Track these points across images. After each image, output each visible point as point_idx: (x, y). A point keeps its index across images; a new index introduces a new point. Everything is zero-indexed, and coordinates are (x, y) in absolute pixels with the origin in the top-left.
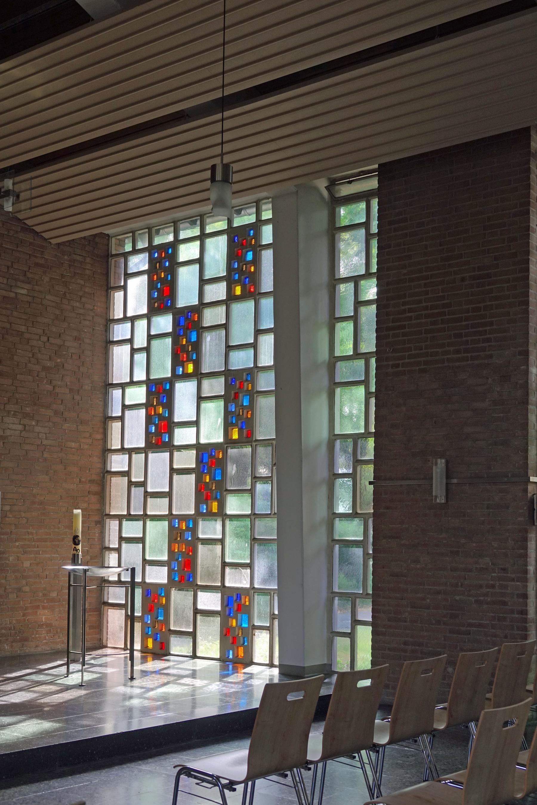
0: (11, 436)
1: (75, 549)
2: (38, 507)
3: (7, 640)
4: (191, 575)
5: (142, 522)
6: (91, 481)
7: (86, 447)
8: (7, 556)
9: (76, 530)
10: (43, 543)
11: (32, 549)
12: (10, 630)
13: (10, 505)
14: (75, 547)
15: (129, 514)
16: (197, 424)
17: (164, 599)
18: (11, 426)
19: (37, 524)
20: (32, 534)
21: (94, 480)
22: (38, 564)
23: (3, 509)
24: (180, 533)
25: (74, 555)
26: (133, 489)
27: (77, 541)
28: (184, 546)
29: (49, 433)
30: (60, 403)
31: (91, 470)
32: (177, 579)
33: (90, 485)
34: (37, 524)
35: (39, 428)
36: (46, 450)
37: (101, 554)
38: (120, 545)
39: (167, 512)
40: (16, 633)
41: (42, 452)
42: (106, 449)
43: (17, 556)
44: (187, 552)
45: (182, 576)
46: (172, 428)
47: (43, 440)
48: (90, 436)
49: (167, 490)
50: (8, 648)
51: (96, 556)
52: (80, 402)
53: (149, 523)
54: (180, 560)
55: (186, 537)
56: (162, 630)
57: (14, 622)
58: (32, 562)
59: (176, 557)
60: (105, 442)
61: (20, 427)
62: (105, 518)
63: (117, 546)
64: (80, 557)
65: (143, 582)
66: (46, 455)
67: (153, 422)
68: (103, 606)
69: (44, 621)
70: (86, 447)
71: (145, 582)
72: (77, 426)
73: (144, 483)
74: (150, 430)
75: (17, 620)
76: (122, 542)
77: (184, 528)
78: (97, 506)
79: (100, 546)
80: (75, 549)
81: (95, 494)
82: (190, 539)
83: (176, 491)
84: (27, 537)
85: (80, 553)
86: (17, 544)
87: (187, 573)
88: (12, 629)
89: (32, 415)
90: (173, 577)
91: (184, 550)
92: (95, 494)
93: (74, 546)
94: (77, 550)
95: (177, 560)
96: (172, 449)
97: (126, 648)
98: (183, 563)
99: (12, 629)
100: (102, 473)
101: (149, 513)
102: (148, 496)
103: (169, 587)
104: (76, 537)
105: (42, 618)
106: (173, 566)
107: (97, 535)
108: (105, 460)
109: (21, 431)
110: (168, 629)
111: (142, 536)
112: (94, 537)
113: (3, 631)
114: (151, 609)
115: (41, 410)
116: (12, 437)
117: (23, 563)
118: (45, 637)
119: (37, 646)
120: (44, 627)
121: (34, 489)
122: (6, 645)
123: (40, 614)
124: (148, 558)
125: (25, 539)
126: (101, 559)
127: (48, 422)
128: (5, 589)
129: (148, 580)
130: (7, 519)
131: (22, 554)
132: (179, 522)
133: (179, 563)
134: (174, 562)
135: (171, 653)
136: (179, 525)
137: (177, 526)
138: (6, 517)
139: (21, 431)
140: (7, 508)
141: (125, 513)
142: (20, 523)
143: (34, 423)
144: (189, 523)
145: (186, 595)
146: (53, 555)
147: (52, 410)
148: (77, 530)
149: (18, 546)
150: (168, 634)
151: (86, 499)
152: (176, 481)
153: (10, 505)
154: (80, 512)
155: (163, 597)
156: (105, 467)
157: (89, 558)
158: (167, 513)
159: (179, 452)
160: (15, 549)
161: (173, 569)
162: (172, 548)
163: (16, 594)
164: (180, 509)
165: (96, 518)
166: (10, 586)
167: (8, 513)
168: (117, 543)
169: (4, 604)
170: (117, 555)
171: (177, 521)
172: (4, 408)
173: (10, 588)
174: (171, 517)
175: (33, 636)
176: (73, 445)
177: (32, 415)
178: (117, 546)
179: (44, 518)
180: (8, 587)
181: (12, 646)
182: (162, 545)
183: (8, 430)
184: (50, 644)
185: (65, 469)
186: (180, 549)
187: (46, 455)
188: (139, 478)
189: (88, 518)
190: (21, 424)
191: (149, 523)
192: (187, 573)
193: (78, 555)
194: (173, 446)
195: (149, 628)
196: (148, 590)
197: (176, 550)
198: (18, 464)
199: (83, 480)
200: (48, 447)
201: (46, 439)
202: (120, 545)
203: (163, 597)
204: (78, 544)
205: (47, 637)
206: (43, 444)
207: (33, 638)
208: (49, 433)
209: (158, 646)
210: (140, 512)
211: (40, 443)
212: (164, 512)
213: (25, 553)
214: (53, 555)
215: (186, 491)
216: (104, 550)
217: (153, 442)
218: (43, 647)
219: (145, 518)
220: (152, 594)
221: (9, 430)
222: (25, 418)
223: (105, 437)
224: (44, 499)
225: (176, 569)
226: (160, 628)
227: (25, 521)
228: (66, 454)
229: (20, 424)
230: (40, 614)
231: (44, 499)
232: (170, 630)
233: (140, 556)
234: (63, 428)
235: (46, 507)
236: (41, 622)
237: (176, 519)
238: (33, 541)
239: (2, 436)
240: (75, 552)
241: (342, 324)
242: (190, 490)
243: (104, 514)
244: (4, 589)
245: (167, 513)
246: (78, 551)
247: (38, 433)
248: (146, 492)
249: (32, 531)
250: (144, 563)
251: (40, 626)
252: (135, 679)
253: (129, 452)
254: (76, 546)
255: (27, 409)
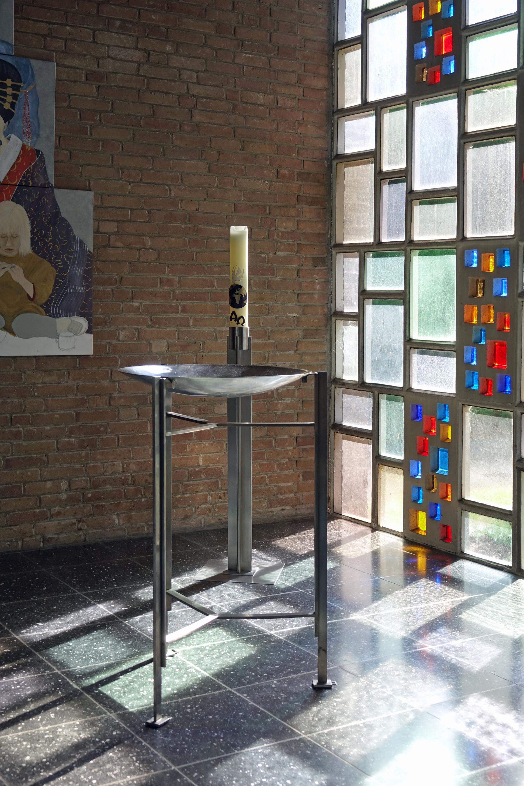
0: (116, 73)
1: (234, 316)
2: (183, 226)
3: (118, 505)
4: (509, 379)
5: (404, 258)
6: (302, 176)
7: (290, 103)
8: (112, 329)
9: (237, 273)
10: (196, 303)
11: (171, 315)
12: (123, 484)
13: (118, 222)
14: (234, 313)
15: (378, 243)
16: (518, 22)
17: (450, 428)
18: (114, 52)
19: (182, 262)
20: (170, 282)
21: (309, 174)
22: (184, 347)
23: (102, 230)
24: (484, 281)
25: (233, 329)
26: (386, 188)
27: (237, 298)
28: (492, 311)
29: (206, 71)
30: (230, 8)
31: (301, 151)
32: (476, 387)
33: (300, 183)
34: (182, 262)
35: (182, 59)
36: (200, 107)
37: (326, 325)
38: (362, 307)
39: (453, 234)
40: (137, 491)
41: (190, 110)
42: (335, 110)
43: (136, 329)
44: (498, 327)
45: (488, 381)
46: (463, 40)
47: (191, 86)
48: (300, 81)
49: (453, 183)
50: (121, 523)
51: (317, 330)
52: (275, 8)
53: (417, 260)
54: (483, 342)
55: (495, 290)
56: (447, 496)
57: (133, 467)
58: (171, 341)
59: (474, 338)
60: (333, 94)
61: (138, 55)
62: (334, 252)
63: (356, 310)
64: (247, 334)
65: (407, 388)
66: (198, 117)
67: (422, 36)
68: (332, 432)
69: (201, 464)
70: (290, 103)
71: (410, 389)
72: (269, 59)
73: (407, 174)
74: (416, 56)
75: (139, 463)
76: (366, 301)
77: (492, 270)
78: (318, 228)
79: (325, 310)
80: (234, 316)
81: (311, 203)
82: (504, 294)
83: (473, 185)
84: (158, 289)
85: (246, 325)
86: (136, 304)
87: (498, 375)
88: (130, 482)
89: (164, 29)
90: (468, 382)
91: (492, 320)
92: (313, 202)
93: (232, 309)
94: (237, 319)
95: (477, 342)
96: (464, 88)
97: (375, 526)
98: (489, 351)
99: (130, 482)
100: (327, 159)
101: (416, 237)
102: (414, 202)
103: (460, 404)
104: (236, 289)
105: (197, 458)
106: (467, 357)
107: (318, 287)
108: (332, 133)
109: (139, 64)
110: (459, 498)
111: (402, 288)
112: (311, 292)
113: (108, 486)
114: (423, 451)
115: (185, 20)
116: (119, 76)
117: (150, 344)
118: (206, 499)
119: (186, 517)
120: (203, 477)
121: (172, 188)
122: (114, 517)
123: (192, 450)
124: (415, 335)
125: (155, 295)
126: (328, 335)
127: (202, 46)
128: (111, 398)
129: (416, 385)
130: (111, 251)
131: (148, 326)
132: (479, 258)
133: (481, 350)
134: (470, 348)
135: (467, 551)
136: (479, 262)
137: (475, 265)
138: (108, 246)
139: (139, 64)
140: (112, 227)
141: (370, 240)
142: (141, 259)
143: (168, 48)
144: (504, 258)
145: (497, 426)
146: (219, 329)
147: (211, 22)
148: (238, 272)
149: (138, 308)
150: (459, 509)
151: (293, 212)
152: (474, 161)
153: (118, 222)
154: (243, 232)
155: (447, 424)
156: (332, 146)
157: (301, 334)
158: (454, 236)
159: (479, 95)
160: (132, 316)
161: (469, 364)
162: (466, 317)
163: (137, 409)
164: (482, 227)
165: (316, 253)
166: (120, 392)
167: (113, 239)
168: (356, 303)
169: (109, 430)
170: (356, 329)
171: (475, 254)
172: (98, 12)
173: (121, 397)
174: (462, 245)
175: (178, 496)
176: (261, 98)
177: (164, 29)
178: (356, 310)
179: (198, 250)
180: (116, 395)
181: (129, 518)
182: (444, 309)
183: (109, 59)
184: (216, 512)
185: (243, 149)
186: (483, 319)
187: (198, 117)
188: (397, 163)
189: (298, 252)
190: (140, 50)
191: (417, 260)
192: (498, 375)
193: (241, 329)
194: (467, 81)
195: (419, 488)
196: (417, 406)
197: (475, 321)
198: (134, 135)
199: (285, 171)
200: (204, 100)
201: (199, 83)
202: (362, 307)
203: (447, 424)
204: (241, 305)
205: (210, 499)
206: (191, 93)
207: (178, 500)
208: (206, 71)
209: (438, 534)
210: (399, 236)
211: (184, 91)
212: (448, 233)
213: (155, 322)
214: (219, 329)
215: (496, 184)
216: (333, 319)
217: (424, 80)
218: (201, 518)
219: (408, 249)
220: (424, 416)
221: (112, 61)
222: (148, 36)
223: (333, 85)
224: (197, 210)
225: (474, 363)
226: (442, 493)
227: (152, 255)
228: (245, 117)
229: (136, 48)
230: (192, 450)
231: (197, 210)
232: (462, 501)
233: (399, 331)
234: (237, 61)
235: (201, 227)
236: (196, 467)
237: (472, 248)
238: (174, 298)
239: (94, 72)
240: (234, 323)
241: (423, 621)
242: (505, 181)
243: (333, 243)
244: (107, 399)
245: (454, 236)
246: (241, 321)
247: (180, 69)
248: (410, 192)
249: (171, 277)
250: (408, 347)
251: (195, 475)
252: (329, 688)
253: (376, 110)
254: (237, 311)
255: (153, 17)
